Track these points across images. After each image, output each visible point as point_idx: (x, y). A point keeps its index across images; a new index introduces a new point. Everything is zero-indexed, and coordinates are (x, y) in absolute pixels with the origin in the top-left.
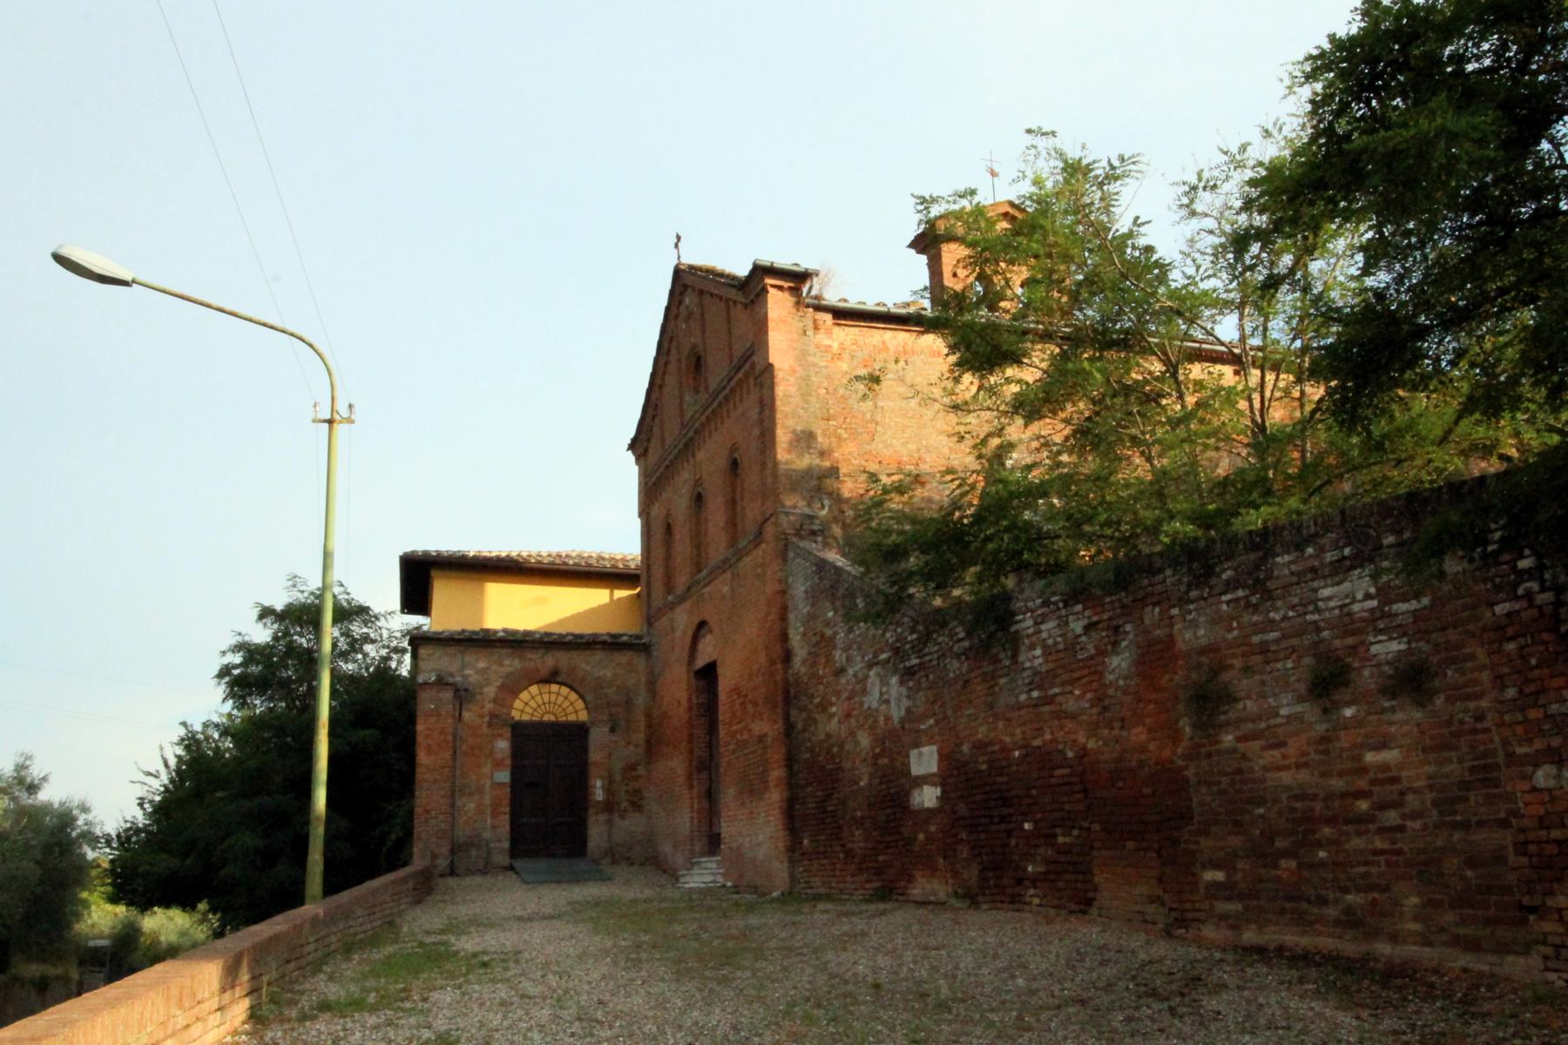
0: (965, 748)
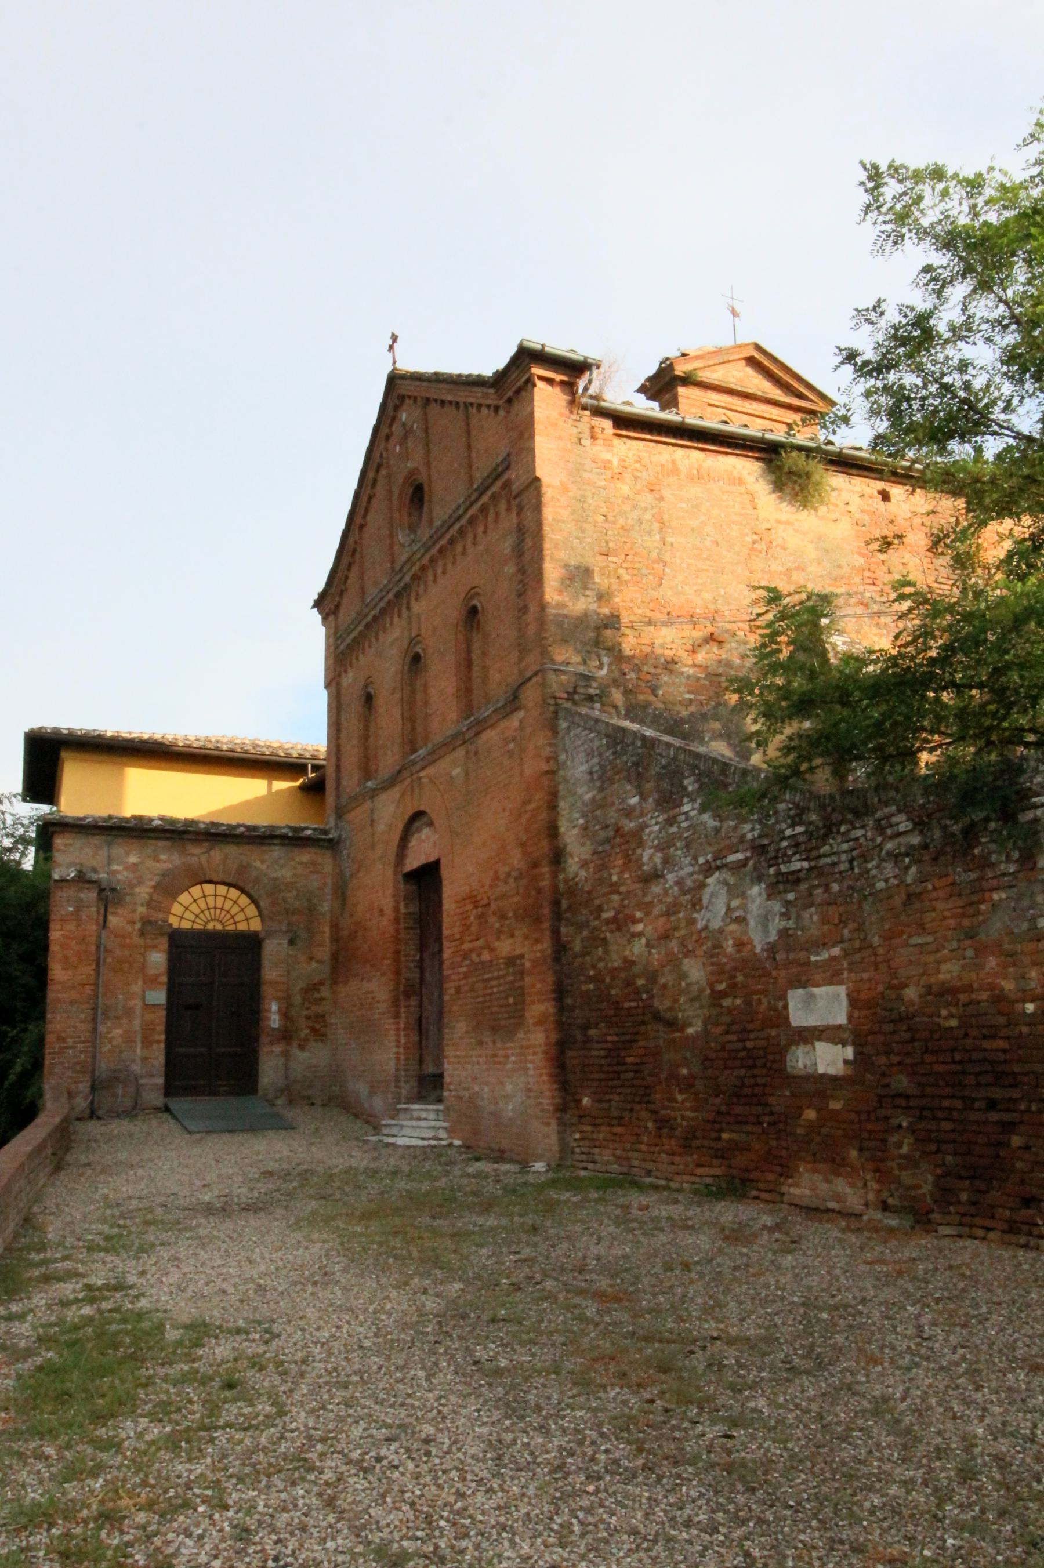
0: (911, 993)
